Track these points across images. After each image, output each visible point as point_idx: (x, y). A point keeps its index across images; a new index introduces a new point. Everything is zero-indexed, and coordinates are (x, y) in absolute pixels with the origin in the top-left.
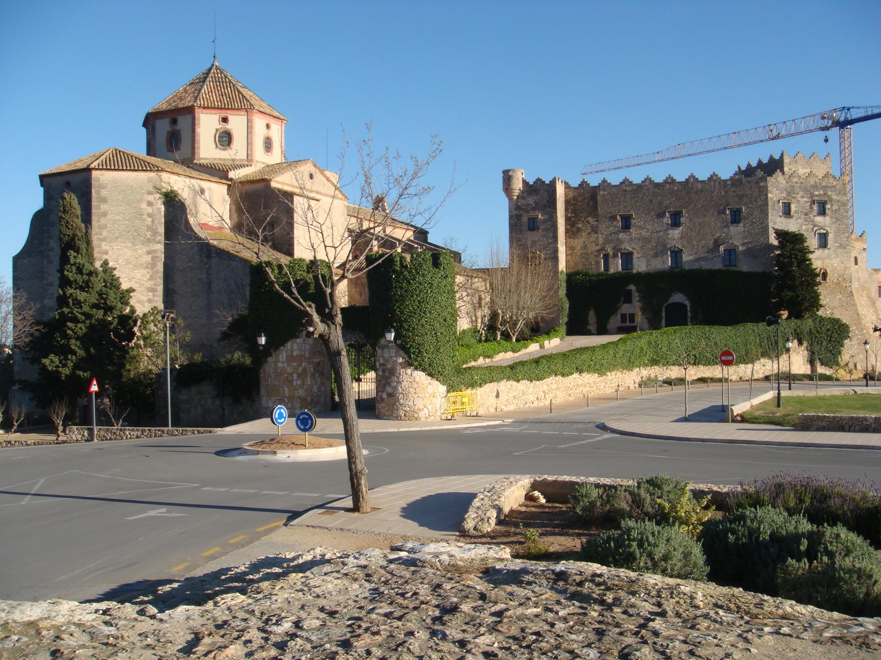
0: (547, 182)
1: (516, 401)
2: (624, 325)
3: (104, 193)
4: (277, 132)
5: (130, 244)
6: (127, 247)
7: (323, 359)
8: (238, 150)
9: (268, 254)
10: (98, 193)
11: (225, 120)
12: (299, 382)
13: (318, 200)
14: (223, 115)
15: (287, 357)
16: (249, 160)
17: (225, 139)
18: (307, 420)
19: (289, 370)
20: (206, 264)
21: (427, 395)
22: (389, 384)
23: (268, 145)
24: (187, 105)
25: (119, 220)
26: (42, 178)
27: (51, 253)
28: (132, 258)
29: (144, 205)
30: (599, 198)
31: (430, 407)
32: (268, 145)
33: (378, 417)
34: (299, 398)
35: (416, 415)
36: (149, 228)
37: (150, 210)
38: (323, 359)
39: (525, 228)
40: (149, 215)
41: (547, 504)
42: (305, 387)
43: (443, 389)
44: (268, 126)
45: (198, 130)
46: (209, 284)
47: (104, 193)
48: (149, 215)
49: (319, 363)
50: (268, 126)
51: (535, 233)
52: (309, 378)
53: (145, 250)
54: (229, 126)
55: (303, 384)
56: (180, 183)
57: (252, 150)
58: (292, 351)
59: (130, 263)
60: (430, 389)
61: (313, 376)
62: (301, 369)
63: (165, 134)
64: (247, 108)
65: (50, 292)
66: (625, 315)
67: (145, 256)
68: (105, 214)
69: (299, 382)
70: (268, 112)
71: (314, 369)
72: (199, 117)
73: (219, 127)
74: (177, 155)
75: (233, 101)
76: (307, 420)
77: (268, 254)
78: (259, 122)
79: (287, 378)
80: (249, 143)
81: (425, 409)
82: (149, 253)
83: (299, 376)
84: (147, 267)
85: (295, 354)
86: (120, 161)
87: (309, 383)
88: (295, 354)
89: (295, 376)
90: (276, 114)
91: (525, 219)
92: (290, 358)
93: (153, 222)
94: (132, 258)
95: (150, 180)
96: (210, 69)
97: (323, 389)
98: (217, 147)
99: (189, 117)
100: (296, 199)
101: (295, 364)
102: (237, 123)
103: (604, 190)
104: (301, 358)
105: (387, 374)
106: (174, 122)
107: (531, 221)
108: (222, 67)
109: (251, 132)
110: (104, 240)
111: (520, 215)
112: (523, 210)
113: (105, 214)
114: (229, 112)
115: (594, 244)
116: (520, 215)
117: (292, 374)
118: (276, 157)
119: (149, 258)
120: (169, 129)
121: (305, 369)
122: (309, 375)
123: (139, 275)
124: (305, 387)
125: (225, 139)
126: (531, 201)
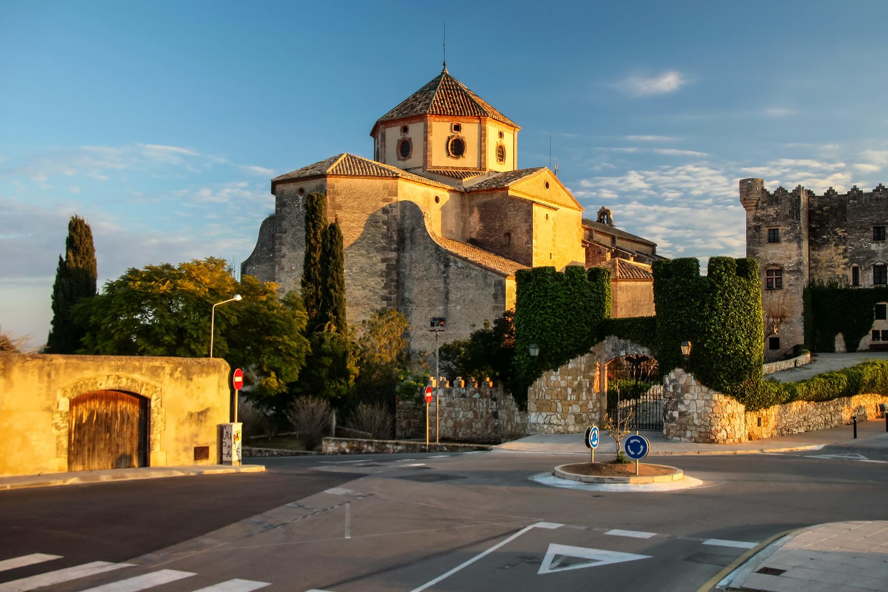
0: (790, 191)
1: (806, 424)
2: (877, 342)
3: (338, 200)
4: (509, 141)
5: (364, 252)
6: (361, 255)
8: (469, 160)
9: (525, 267)
10: (333, 199)
11: (457, 128)
13: (556, 209)
14: (455, 123)
16: (482, 167)
17: (457, 148)
18: (639, 445)
20: (444, 273)
21: (725, 415)
22: (682, 403)
23: (501, 154)
25: (353, 228)
27: (282, 260)
28: (366, 266)
30: (848, 207)
31: (728, 429)
32: (501, 154)
33: (666, 439)
34: (574, 414)
35: (713, 437)
36: (384, 236)
39: (766, 240)
40: (384, 223)
41: (701, 539)
43: (742, 408)
44: (501, 135)
45: (430, 138)
46: (447, 294)
47: (338, 200)
48: (384, 223)
50: (501, 135)
51: (776, 245)
54: (461, 134)
55: (578, 399)
56: (412, 190)
57: (485, 158)
59: (364, 271)
60: (729, 409)
62: (576, 383)
63: (396, 143)
64: (478, 113)
66: (878, 331)
67: (380, 264)
69: (574, 397)
70: (502, 119)
72: (431, 125)
73: (450, 134)
74: (409, 163)
75: (465, 106)
76: (632, 445)
77: (525, 267)
78: (492, 130)
80: (482, 151)
81: (723, 431)
82: (383, 261)
83: (574, 391)
84: (381, 276)
86: (355, 167)
87: (584, 398)
89: (570, 391)
90: (509, 122)
91: (765, 231)
93: (388, 230)
94: (366, 266)
95: (385, 188)
96: (440, 77)
98: (449, 155)
99: (421, 125)
100: (535, 208)
101: (570, 378)
102: (469, 131)
103: (854, 199)
105: (679, 391)
106: (405, 130)
107: (772, 232)
108: (452, 75)
109: (485, 140)
111: (759, 227)
112: (763, 220)
114: (461, 119)
115: (842, 257)
116: (759, 227)
117: (566, 389)
118: (508, 166)
119: (383, 266)
120: (400, 137)
121: (580, 384)
123: (373, 283)
125: (457, 148)
126: (771, 211)
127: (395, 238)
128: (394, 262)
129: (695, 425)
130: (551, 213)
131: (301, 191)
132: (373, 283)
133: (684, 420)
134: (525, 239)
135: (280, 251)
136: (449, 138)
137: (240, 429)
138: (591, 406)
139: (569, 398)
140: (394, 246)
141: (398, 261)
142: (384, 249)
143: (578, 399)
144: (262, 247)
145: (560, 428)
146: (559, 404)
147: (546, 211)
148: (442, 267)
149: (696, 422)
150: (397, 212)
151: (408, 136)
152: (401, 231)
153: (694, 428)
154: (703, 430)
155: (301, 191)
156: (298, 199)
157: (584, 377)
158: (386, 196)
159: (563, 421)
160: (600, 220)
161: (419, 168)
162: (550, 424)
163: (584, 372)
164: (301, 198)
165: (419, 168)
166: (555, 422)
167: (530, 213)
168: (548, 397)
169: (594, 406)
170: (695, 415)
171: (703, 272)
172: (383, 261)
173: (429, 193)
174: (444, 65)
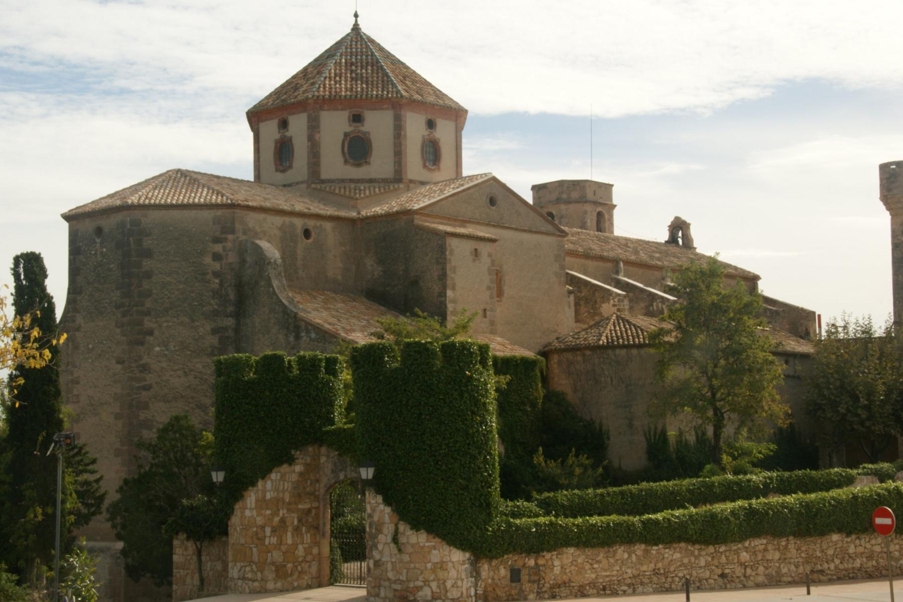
5: (186, 320)
7: (315, 504)
11: (357, 119)
12: (274, 540)
13: (493, 241)
14: (356, 111)
15: (257, 501)
19: (260, 521)
24: (299, 98)
26: (67, 217)
27: (77, 334)
29: (208, 260)
34: (273, 563)
37: (217, 266)
38: (315, 504)
40: (216, 274)
42: (283, 548)
44: (431, 124)
49: (309, 511)
52: (289, 534)
53: (208, 328)
58: (264, 492)
61: (297, 529)
62: (277, 519)
65: (75, 392)
68: (148, 275)
69: (274, 540)
71: (300, 521)
73: (349, 129)
79: (257, 533)
80: (399, 153)
82: (214, 331)
83: (274, 531)
85: (268, 496)
87: (290, 541)
88: (268, 496)
89: (268, 530)
92: (262, 503)
93: (221, 284)
97: (315, 551)
101: (268, 512)
104: (277, 503)
110: (148, 313)
113: (148, 275)
117: (263, 528)
119: (214, 340)
120: (277, 136)
121: (283, 521)
122: (290, 529)
123: (199, 366)
124: (283, 548)
127: (232, 296)
128: (231, 333)
129: (389, 579)
130: (484, 248)
131: (99, 231)
132: (199, 366)
133: (377, 572)
134: (436, 289)
135: (74, 321)
136: (346, 135)
137: (230, 571)
138: (300, 551)
139: (267, 542)
140: (231, 309)
141: (237, 330)
142: (215, 314)
143: (280, 542)
144: (69, 312)
145: (256, 584)
146: (255, 550)
147: (469, 245)
148: (292, 339)
149: (390, 575)
150: (232, 258)
151: (288, 134)
152: (239, 287)
153: (387, 583)
154: (398, 587)
155: (99, 231)
156: (95, 243)
157: (289, 510)
158: (217, 234)
159: (259, 575)
160: (673, 240)
161: (302, 182)
162: (244, 578)
163: (290, 503)
164: (98, 241)
165: (302, 182)
166: (249, 575)
167: (442, 249)
168: (242, 541)
169: (308, 551)
170: (389, 566)
171: (296, 372)
172: (214, 331)
173: (292, 225)
174: (356, 16)
